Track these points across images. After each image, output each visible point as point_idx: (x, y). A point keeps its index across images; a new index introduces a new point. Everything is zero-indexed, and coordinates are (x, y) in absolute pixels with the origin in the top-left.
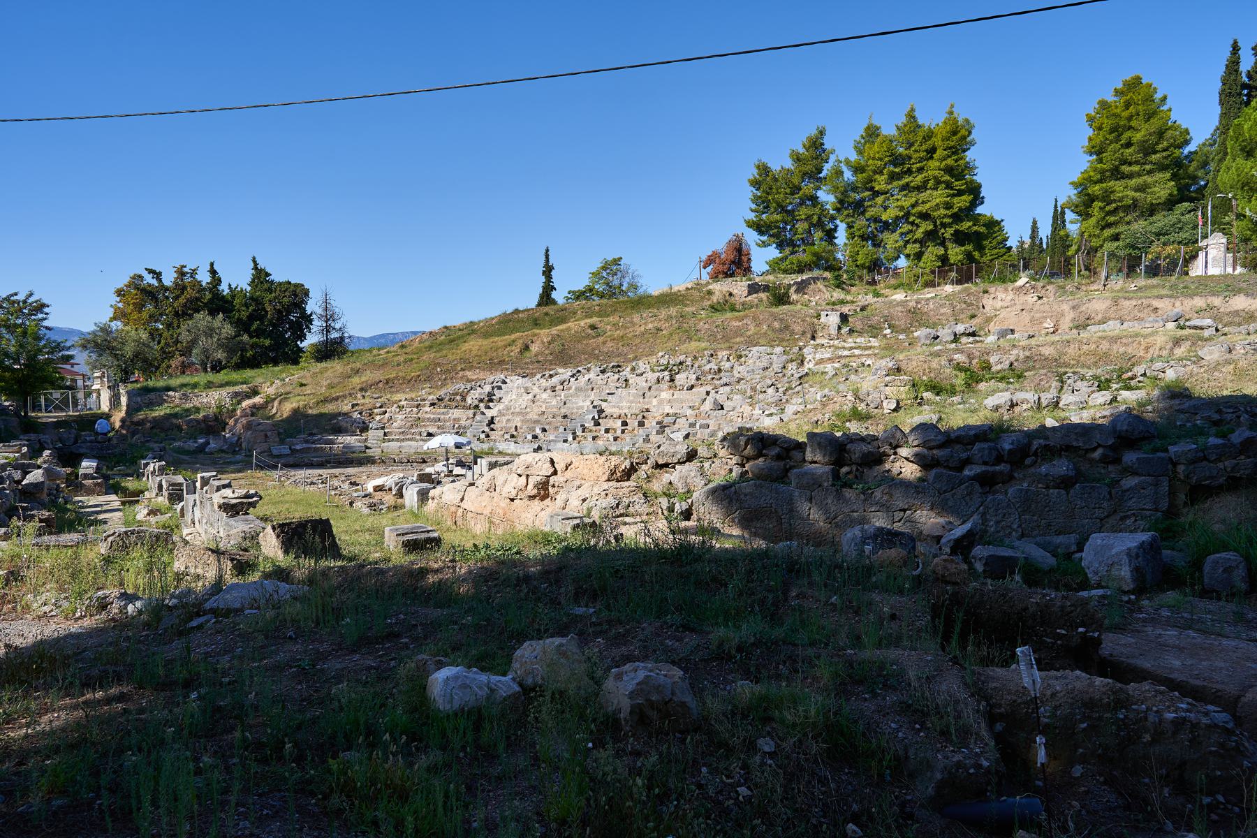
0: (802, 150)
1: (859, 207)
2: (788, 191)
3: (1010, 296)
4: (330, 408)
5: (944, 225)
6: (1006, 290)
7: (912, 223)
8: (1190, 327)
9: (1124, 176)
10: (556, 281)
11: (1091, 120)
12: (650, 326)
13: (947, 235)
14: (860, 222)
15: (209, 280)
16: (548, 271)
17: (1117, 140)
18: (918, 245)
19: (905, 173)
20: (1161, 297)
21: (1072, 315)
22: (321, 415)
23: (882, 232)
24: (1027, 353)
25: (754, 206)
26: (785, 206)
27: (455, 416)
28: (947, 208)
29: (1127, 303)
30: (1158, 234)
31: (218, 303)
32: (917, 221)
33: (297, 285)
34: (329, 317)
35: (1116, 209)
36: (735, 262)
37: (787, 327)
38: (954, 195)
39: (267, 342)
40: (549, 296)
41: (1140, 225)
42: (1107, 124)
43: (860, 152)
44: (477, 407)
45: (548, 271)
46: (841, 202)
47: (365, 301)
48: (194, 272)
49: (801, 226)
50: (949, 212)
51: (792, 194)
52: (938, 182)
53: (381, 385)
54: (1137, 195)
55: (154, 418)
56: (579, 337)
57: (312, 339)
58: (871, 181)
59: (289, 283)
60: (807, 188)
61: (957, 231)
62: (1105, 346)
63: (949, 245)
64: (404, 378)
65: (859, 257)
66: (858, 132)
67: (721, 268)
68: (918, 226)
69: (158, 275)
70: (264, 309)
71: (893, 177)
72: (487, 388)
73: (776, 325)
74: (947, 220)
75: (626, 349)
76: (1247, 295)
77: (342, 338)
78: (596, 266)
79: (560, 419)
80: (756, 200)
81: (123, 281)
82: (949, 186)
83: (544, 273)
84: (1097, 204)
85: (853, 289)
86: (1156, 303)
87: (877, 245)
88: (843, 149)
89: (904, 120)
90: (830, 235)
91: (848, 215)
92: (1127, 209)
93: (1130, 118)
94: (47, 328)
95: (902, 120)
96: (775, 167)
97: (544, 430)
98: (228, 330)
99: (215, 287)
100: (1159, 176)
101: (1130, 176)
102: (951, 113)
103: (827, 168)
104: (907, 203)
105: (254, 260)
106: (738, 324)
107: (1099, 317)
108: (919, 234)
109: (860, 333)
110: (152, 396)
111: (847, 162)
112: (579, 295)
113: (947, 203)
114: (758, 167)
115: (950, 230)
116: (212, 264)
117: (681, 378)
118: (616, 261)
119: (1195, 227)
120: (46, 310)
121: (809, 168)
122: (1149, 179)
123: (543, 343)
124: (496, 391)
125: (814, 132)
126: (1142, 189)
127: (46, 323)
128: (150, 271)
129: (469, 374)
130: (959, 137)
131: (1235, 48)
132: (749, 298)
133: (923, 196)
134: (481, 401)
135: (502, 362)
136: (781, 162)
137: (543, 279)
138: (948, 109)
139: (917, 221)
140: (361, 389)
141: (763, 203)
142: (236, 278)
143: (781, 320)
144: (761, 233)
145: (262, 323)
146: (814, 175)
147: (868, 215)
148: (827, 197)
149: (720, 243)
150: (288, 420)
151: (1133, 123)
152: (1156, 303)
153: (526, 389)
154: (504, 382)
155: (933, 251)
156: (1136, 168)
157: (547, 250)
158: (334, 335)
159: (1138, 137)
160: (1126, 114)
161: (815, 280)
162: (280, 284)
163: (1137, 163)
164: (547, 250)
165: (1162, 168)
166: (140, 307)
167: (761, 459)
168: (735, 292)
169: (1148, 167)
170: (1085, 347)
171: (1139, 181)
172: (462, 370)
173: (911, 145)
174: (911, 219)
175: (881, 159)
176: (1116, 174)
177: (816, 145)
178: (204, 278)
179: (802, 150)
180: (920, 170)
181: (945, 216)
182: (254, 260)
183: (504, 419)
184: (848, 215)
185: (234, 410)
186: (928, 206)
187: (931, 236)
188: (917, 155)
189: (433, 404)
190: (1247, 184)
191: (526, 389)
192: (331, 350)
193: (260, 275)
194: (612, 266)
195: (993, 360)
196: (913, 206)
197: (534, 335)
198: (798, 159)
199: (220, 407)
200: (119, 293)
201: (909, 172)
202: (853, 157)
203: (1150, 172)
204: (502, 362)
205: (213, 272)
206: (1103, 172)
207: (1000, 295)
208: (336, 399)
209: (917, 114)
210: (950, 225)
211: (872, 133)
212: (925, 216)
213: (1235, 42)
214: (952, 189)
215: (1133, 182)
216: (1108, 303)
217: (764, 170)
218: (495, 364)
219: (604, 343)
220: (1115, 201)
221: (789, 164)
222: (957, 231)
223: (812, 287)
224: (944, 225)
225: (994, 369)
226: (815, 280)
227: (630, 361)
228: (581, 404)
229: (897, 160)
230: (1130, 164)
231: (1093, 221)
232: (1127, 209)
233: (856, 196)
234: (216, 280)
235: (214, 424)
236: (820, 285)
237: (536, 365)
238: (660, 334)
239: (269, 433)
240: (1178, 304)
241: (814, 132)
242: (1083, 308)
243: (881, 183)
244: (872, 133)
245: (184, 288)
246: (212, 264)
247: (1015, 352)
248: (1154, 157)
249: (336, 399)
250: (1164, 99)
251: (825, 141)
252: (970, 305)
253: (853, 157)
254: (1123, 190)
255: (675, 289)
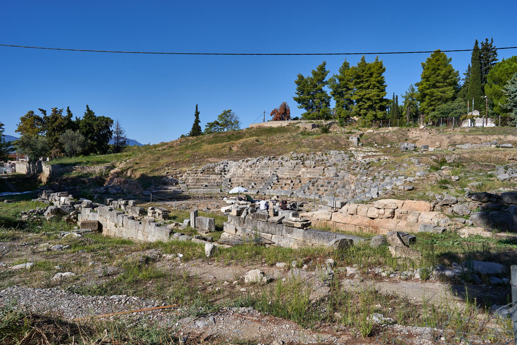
0: (317, 71)
1: (341, 94)
2: (312, 86)
3: (418, 132)
4: (156, 174)
5: (376, 103)
6: (416, 130)
7: (364, 102)
8: (502, 147)
9: (437, 87)
10: (201, 118)
11: (423, 65)
12: (282, 141)
13: (377, 107)
14: (342, 100)
15: (67, 115)
16: (197, 114)
17: (435, 73)
18: (365, 110)
19: (361, 82)
20: (481, 135)
21: (448, 140)
22: (154, 177)
23: (350, 104)
24: (459, 156)
25: (297, 92)
26: (309, 93)
27: (213, 178)
28: (378, 96)
29: (469, 137)
30: (452, 109)
31: (74, 126)
32: (366, 101)
33: (108, 118)
34: (119, 132)
35: (435, 99)
36: (283, 114)
37: (338, 142)
38: (380, 92)
39: (95, 143)
40: (197, 124)
41: (444, 106)
42: (431, 67)
43: (341, 73)
44: (221, 174)
45: (197, 114)
46: (334, 92)
47: (149, 126)
48: (61, 111)
49: (317, 101)
50: (378, 98)
51: (313, 87)
52: (374, 86)
53: (174, 164)
54: (442, 94)
55: (72, 178)
56: (252, 145)
57: (111, 143)
58: (346, 84)
59: (104, 117)
60: (319, 86)
61: (381, 105)
62: (488, 154)
63: (377, 111)
64: (183, 161)
65: (342, 114)
66: (341, 65)
67: (279, 116)
68: (366, 103)
69: (44, 112)
70: (93, 129)
71: (357, 83)
72: (222, 166)
73: (334, 141)
74: (377, 101)
75: (274, 150)
76: (513, 135)
77: (125, 141)
78: (221, 112)
79: (260, 179)
80: (299, 89)
81: (24, 114)
82: (378, 88)
83: (195, 115)
84: (427, 97)
85: (347, 127)
86: (480, 137)
87: (347, 109)
88: (333, 71)
89: (361, 61)
90: (328, 104)
91: (337, 97)
92: (439, 100)
93: (439, 65)
94: (4, 136)
95: (360, 61)
96: (306, 77)
97: (255, 184)
98: (82, 138)
99: (70, 118)
100: (449, 88)
101: (439, 87)
102: (377, 60)
103: (327, 79)
104: (362, 94)
105: (87, 107)
106: (317, 141)
107: (459, 142)
108: (366, 106)
109: (366, 145)
110: (68, 168)
111: (337, 76)
112: (211, 125)
113: (378, 95)
114: (299, 76)
115: (379, 105)
116: (68, 108)
117: (307, 163)
118: (229, 111)
119: (466, 107)
120: (3, 127)
121: (320, 77)
122: (445, 88)
123: (238, 146)
124: (225, 167)
125: (322, 64)
126: (443, 92)
127: (4, 133)
128: (41, 110)
129: (210, 159)
130: (381, 69)
131: (477, 43)
132: (312, 130)
133: (368, 91)
134: (221, 171)
135: (223, 155)
136: (308, 75)
137: (195, 118)
138: (376, 58)
139: (366, 101)
140: (166, 166)
141: (301, 91)
142: (79, 114)
143: (335, 140)
144: (299, 103)
145: (92, 134)
146: (321, 81)
147: (345, 97)
148: (328, 90)
149: (277, 106)
150: (139, 179)
151: (440, 68)
152: (480, 137)
153: (239, 166)
154: (228, 163)
155: (371, 113)
156: (441, 84)
157: (197, 106)
158: (121, 140)
159: (442, 73)
160: (437, 64)
161: (334, 123)
162: (99, 117)
163: (441, 82)
164: (197, 106)
165: (450, 85)
166: (32, 126)
167: (489, 203)
168: (307, 127)
169: (445, 84)
170: (481, 155)
171: (443, 89)
172: (207, 158)
173: (363, 71)
174: (363, 100)
175: (352, 76)
176: (434, 86)
177: (322, 68)
178: (65, 114)
179: (317, 71)
180: (367, 81)
181: (377, 99)
182: (87, 107)
183: (235, 179)
184: (337, 97)
185: (108, 174)
186: (370, 95)
187: (371, 107)
188: (366, 75)
189: (202, 173)
190: (497, 94)
191: (239, 166)
192: (120, 147)
193: (90, 114)
194: (226, 114)
195: (447, 158)
196: (364, 95)
197: (233, 143)
198: (315, 74)
199: (102, 173)
200: (23, 119)
201: (362, 82)
202: (339, 74)
203: (446, 86)
204: (223, 155)
205: (69, 111)
206: (430, 85)
207: (415, 132)
208: (157, 170)
209: (365, 59)
210: (378, 103)
211: (346, 65)
212: (369, 99)
213: (477, 41)
214: (379, 89)
215: (441, 89)
216: (462, 136)
217: (301, 77)
218: (221, 156)
219: (264, 147)
220: (434, 96)
221: (311, 76)
222: (381, 105)
223: (333, 126)
224: (376, 103)
225: (448, 162)
226: (334, 123)
227: (280, 155)
228: (266, 173)
229: (358, 77)
230: (439, 82)
231: (425, 103)
232: (439, 100)
233: (340, 90)
234: (70, 115)
235: (100, 181)
236: (335, 125)
237: (238, 156)
238: (287, 144)
239: (138, 185)
240: (488, 137)
241: (321, 64)
242: (452, 138)
243: (351, 85)
244: (346, 65)
245: (57, 119)
246: (68, 108)
247: (454, 156)
248: (448, 81)
249: (157, 170)
250: (451, 59)
251: (326, 67)
252: (404, 135)
253: (339, 74)
254: (437, 92)
255: (283, 125)
